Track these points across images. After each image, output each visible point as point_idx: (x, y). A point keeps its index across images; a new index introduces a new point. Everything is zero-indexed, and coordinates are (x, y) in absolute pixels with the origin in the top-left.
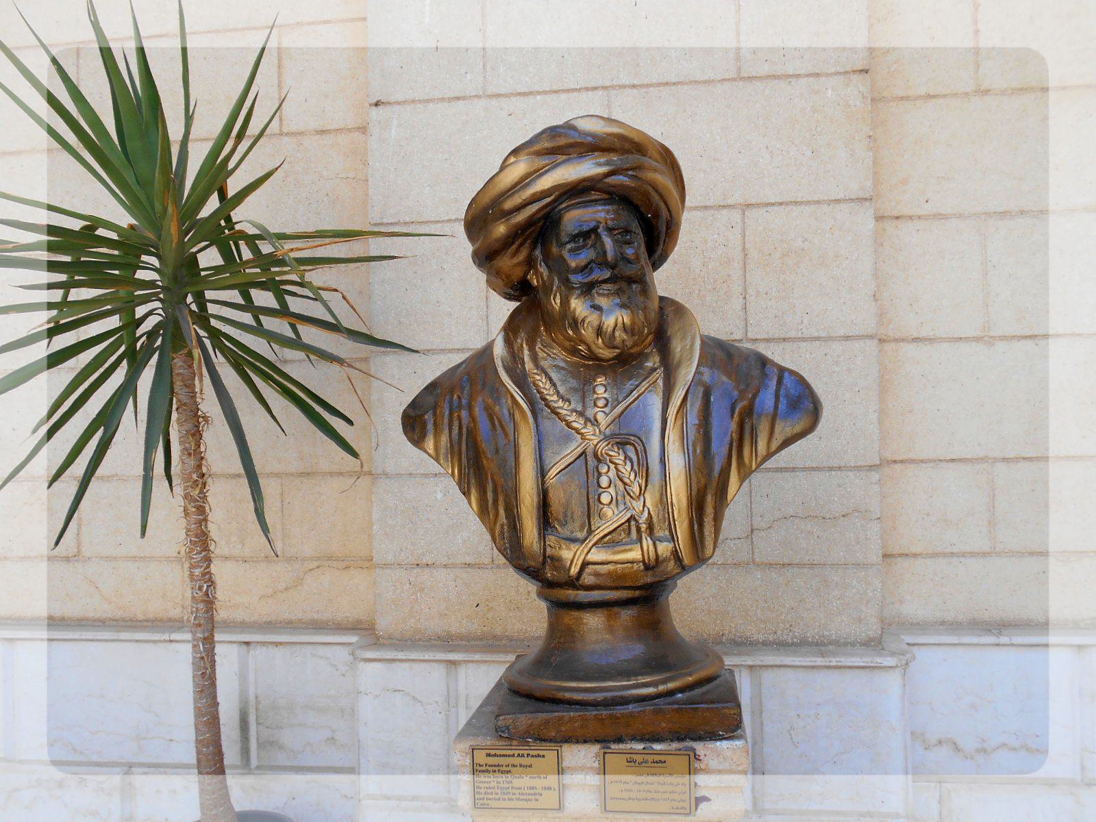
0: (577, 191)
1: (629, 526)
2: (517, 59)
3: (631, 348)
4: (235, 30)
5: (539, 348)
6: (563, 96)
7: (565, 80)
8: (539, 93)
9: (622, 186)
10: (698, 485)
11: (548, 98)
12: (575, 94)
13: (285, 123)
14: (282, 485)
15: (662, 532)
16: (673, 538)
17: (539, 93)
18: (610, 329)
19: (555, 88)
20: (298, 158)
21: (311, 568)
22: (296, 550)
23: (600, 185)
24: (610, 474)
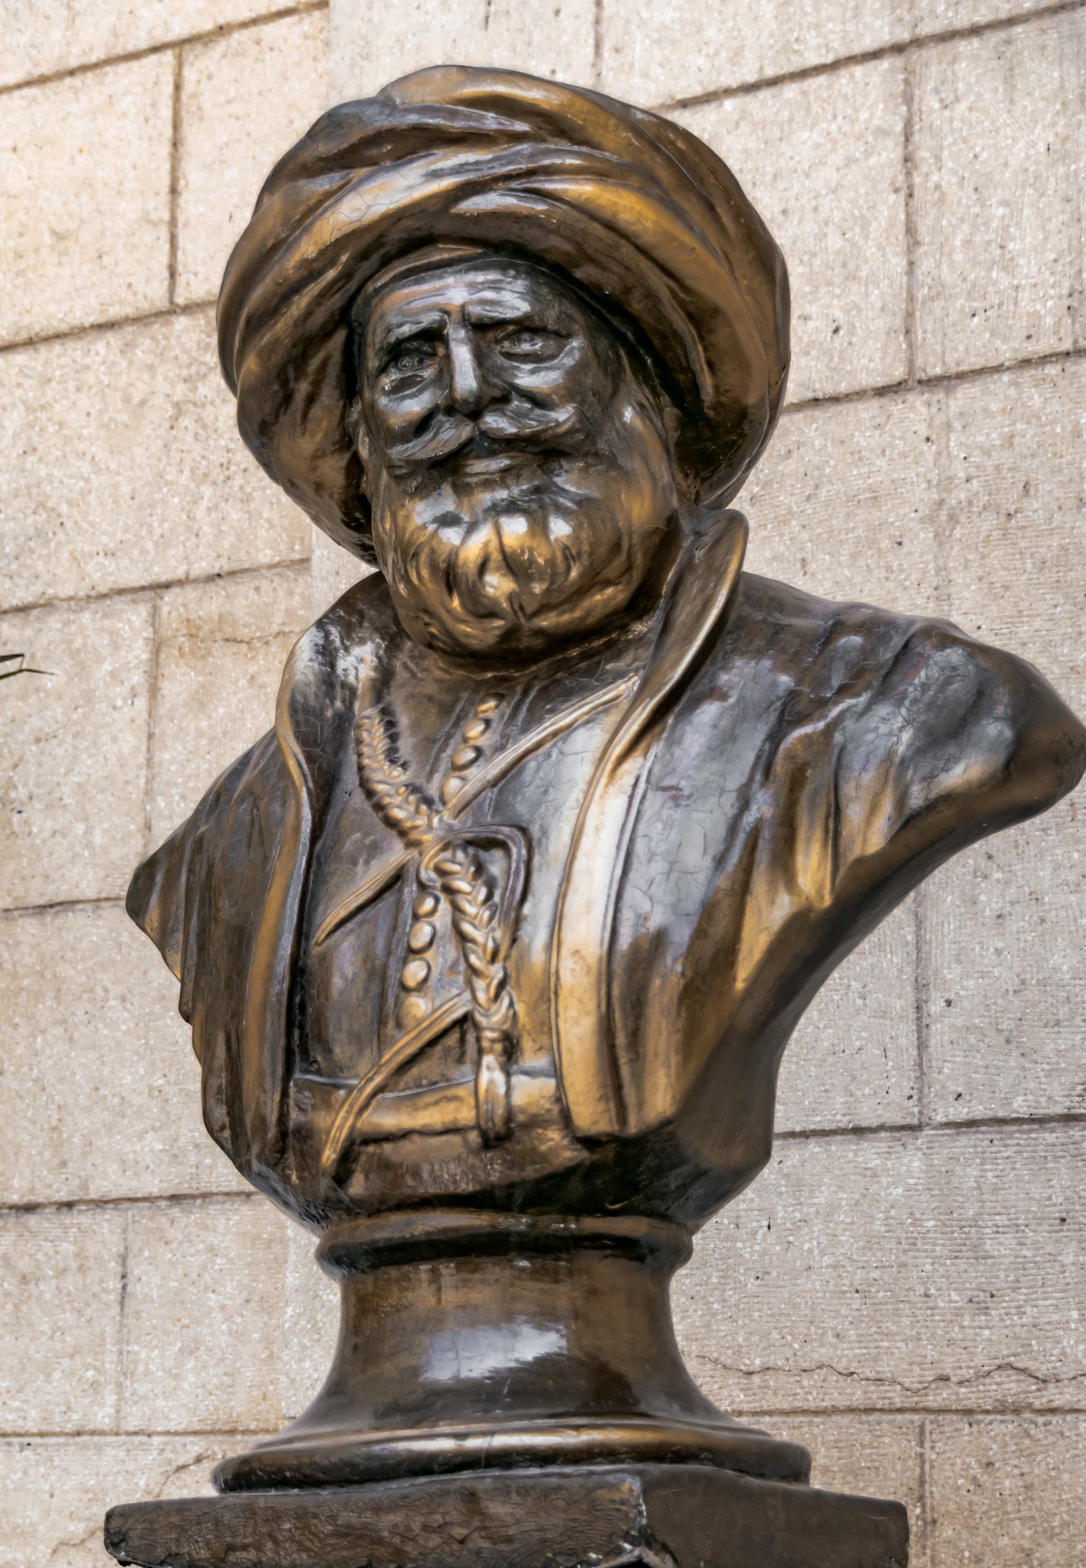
0: (408, 242)
1: (462, 1041)
2: (677, 15)
3: (537, 613)
4: (84, 68)
5: (405, 666)
6: (790, 91)
7: (796, 47)
8: (728, 92)
9: (495, 215)
10: (636, 930)
11: (750, 102)
12: (822, 79)
13: (181, 280)
14: (124, 1231)
15: (532, 1058)
16: (556, 1072)
17: (728, 92)
18: (472, 568)
19: (770, 72)
20: (205, 364)
21: (181, 1462)
22: (148, 1412)
23: (442, 226)
24: (437, 920)
